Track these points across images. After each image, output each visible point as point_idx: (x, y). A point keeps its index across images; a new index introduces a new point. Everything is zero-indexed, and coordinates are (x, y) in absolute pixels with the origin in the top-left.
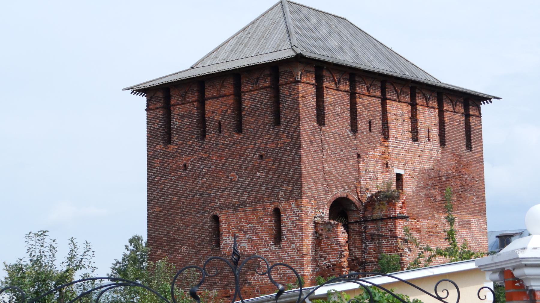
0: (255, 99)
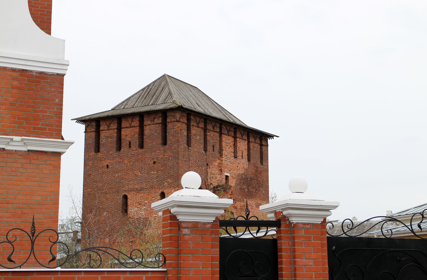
0: (152, 129)
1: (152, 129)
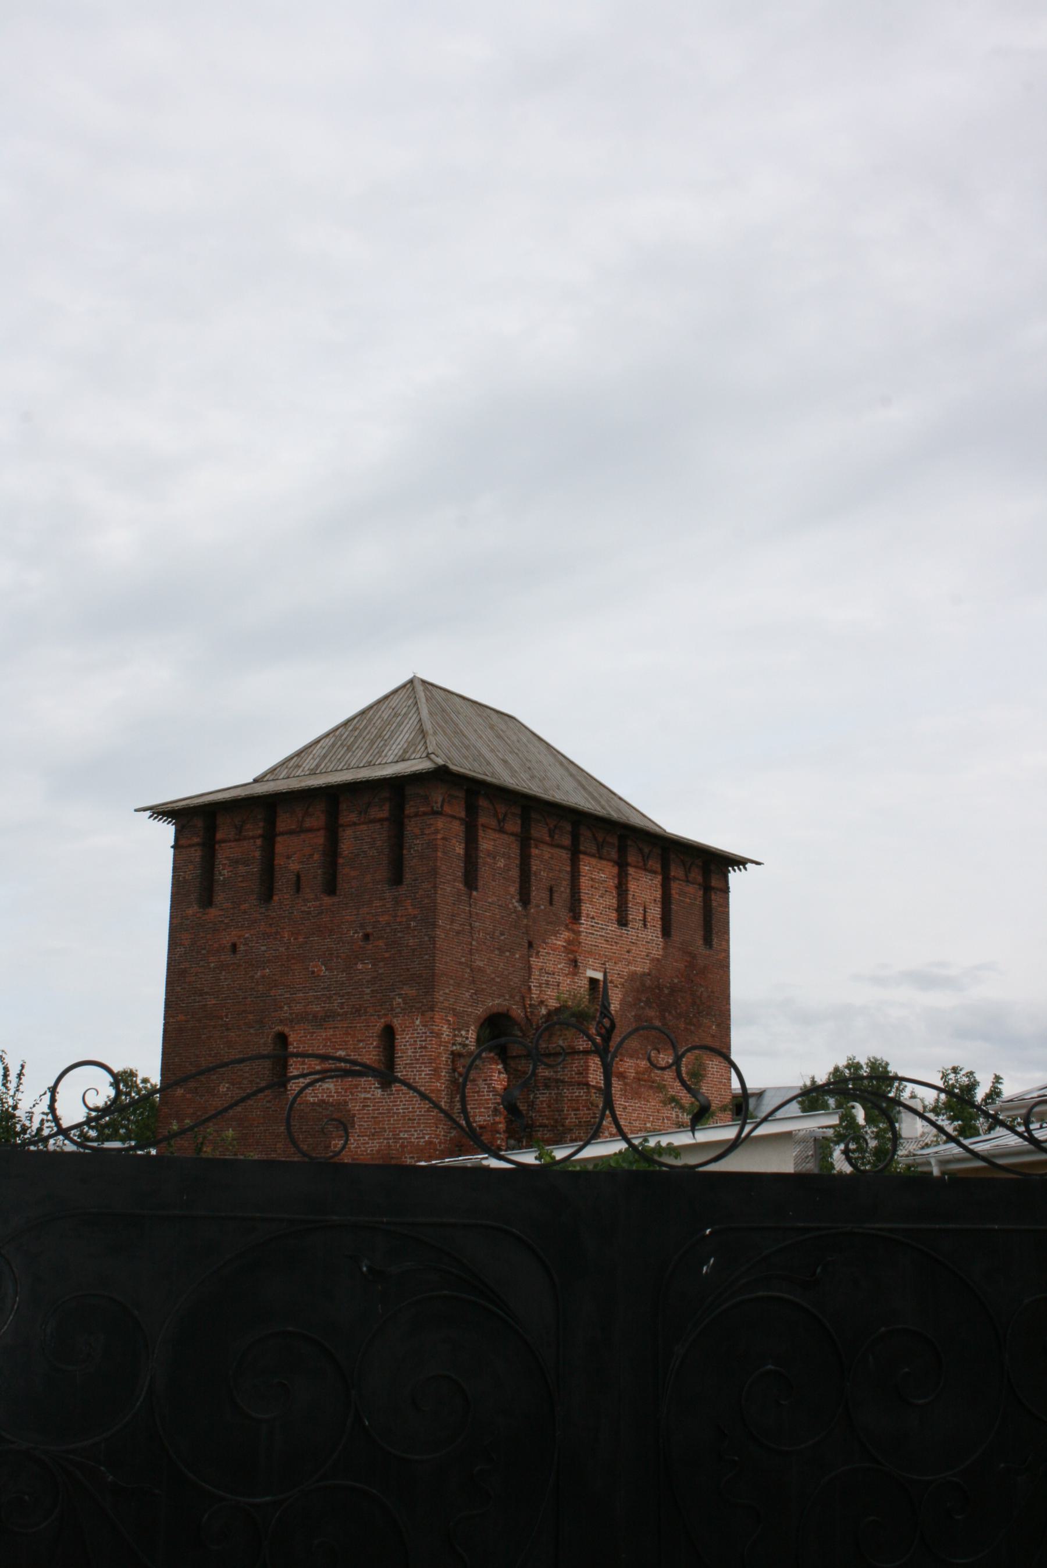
0: (362, 838)
1: (362, 838)
